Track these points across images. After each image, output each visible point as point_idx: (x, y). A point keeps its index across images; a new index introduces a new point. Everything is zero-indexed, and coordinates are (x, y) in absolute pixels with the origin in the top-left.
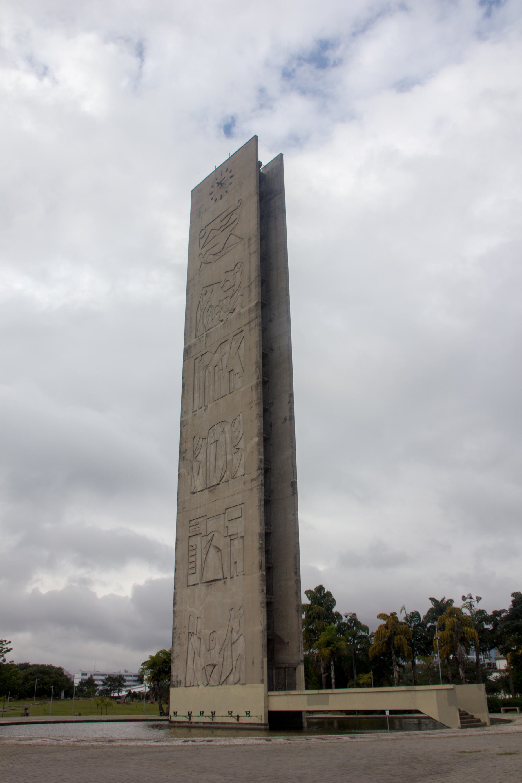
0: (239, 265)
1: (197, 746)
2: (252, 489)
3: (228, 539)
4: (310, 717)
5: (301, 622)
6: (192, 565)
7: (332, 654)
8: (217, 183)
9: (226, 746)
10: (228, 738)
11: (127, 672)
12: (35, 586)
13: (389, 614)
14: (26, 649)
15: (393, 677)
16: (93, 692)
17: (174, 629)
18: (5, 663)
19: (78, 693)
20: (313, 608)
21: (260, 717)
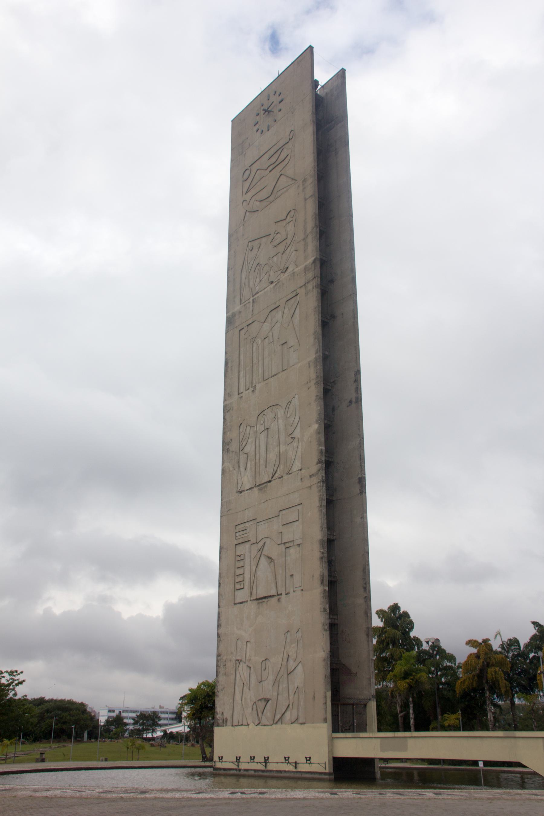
0: (292, 214)
1: (247, 798)
2: (311, 486)
3: (283, 547)
4: (384, 765)
5: (371, 648)
6: (240, 579)
7: (410, 687)
8: (263, 110)
9: (282, 800)
10: (284, 790)
11: (163, 708)
12: (50, 604)
13: (480, 641)
14: (39, 681)
15: (487, 720)
16: (122, 733)
17: (218, 655)
18: (17, 698)
19: (104, 734)
20: (386, 632)
21: (323, 765)
